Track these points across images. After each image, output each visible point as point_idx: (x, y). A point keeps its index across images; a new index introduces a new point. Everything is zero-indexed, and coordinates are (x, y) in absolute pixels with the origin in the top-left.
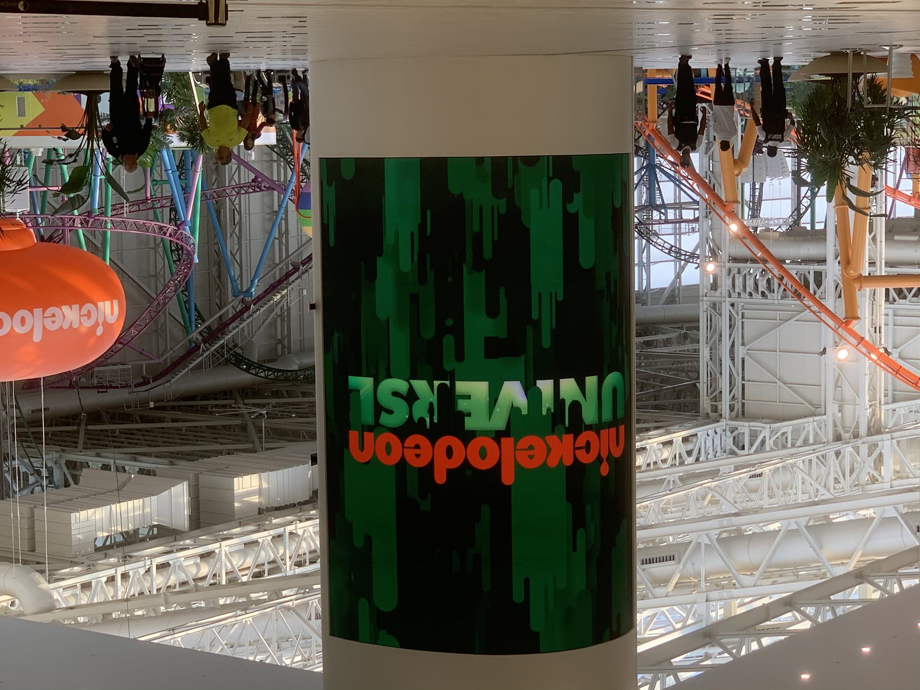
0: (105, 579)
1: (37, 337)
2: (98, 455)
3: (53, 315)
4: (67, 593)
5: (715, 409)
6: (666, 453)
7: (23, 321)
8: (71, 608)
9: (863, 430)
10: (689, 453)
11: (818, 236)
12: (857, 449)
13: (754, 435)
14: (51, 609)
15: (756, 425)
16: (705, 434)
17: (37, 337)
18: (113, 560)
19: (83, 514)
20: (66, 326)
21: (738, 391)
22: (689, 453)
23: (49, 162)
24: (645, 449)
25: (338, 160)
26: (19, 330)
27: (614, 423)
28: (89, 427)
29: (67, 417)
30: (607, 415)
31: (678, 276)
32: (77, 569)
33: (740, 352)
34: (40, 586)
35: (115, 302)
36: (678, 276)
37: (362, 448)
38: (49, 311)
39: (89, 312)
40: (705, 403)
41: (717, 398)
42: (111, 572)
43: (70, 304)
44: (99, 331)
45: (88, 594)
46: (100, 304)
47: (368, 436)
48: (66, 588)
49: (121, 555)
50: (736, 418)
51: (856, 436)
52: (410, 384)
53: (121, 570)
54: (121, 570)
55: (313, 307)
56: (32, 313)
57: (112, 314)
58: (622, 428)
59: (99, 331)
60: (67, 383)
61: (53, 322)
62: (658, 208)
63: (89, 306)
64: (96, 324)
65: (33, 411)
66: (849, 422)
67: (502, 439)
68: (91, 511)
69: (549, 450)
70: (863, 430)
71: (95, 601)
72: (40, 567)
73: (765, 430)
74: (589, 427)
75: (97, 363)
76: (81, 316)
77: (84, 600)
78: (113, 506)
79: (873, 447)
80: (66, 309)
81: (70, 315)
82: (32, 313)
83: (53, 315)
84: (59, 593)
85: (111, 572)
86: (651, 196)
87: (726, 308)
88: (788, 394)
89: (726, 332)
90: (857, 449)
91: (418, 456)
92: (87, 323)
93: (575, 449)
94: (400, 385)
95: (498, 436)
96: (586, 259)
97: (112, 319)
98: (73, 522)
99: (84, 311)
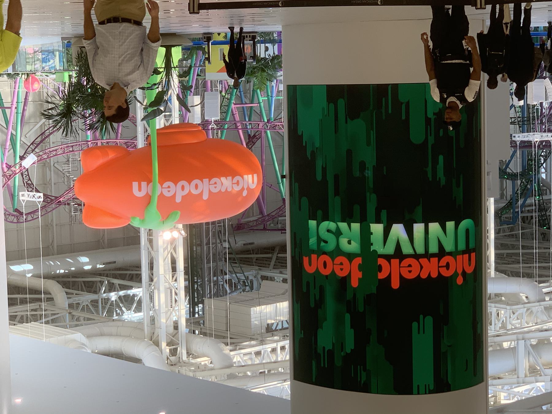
0: (270, 350)
1: (205, 197)
2: (281, 273)
3: (215, 183)
4: (246, 358)
7: (196, 187)
8: (243, 366)
14: (230, 366)
17: (205, 197)
18: (276, 338)
19: (258, 309)
20: (223, 190)
24: (470, 266)
25: (397, 85)
26: (194, 192)
27: (468, 251)
28: (279, 255)
29: (265, 249)
30: (462, 246)
32: (253, 342)
34: (224, 352)
35: (255, 176)
37: (310, 265)
39: (238, 181)
42: (274, 345)
43: (226, 176)
44: (245, 193)
45: (259, 358)
46: (245, 177)
47: (314, 257)
48: (245, 354)
49: (281, 335)
52: (337, 225)
55: (283, 177)
56: (202, 182)
57: (253, 183)
58: (473, 255)
59: (245, 193)
60: (262, 227)
61: (215, 187)
63: (238, 178)
64: (243, 189)
65: (244, 244)
67: (392, 260)
68: (263, 307)
69: (422, 267)
71: (264, 362)
72: (225, 340)
74: (450, 254)
75: (244, 214)
76: (233, 184)
77: (257, 361)
78: (278, 304)
80: (223, 179)
81: (225, 183)
82: (202, 182)
83: (215, 183)
84: (240, 357)
85: (274, 345)
91: (410, 272)
92: (237, 188)
93: (439, 267)
94: (332, 225)
95: (388, 258)
97: (253, 186)
98: (252, 313)
99: (235, 180)
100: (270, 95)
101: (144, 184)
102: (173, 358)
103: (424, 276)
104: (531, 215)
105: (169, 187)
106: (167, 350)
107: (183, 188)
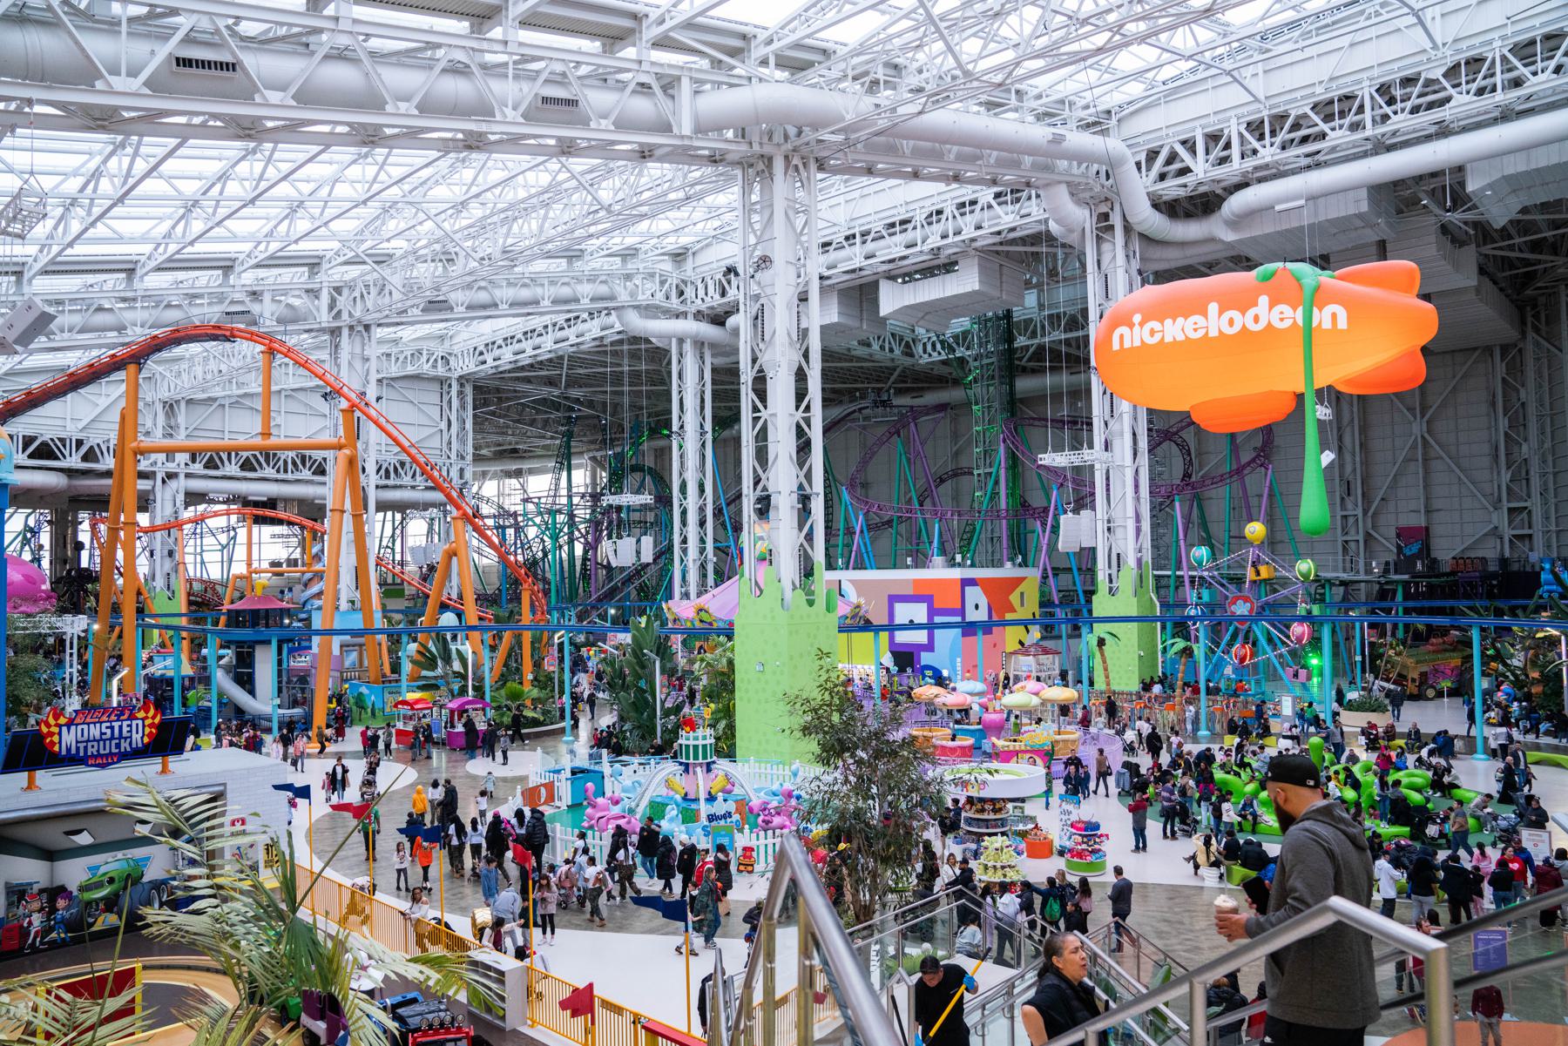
1: (1213, 308)
5: (462, 385)
6: (497, 352)
7: (1231, 322)
9: (345, 332)
10: (481, 353)
11: (382, 507)
12: (350, 315)
13: (434, 366)
15: (432, 373)
16: (468, 366)
17: (1213, 308)
21: (446, 398)
22: (481, 353)
26: (1235, 314)
33: (444, 425)
38: (1200, 333)
40: (469, 390)
41: (460, 393)
44: (1137, 318)
51: (351, 328)
53: (950, 240)
54: (950, 240)
64: (1142, 324)
70: (345, 332)
73: (426, 368)
86: (504, 534)
87: (453, 456)
88: (410, 395)
89: (454, 439)
90: (350, 315)
96: (565, 474)
99: (1158, 337)
102: (1104, 209)
103: (1180, 320)
107: (1256, 319)
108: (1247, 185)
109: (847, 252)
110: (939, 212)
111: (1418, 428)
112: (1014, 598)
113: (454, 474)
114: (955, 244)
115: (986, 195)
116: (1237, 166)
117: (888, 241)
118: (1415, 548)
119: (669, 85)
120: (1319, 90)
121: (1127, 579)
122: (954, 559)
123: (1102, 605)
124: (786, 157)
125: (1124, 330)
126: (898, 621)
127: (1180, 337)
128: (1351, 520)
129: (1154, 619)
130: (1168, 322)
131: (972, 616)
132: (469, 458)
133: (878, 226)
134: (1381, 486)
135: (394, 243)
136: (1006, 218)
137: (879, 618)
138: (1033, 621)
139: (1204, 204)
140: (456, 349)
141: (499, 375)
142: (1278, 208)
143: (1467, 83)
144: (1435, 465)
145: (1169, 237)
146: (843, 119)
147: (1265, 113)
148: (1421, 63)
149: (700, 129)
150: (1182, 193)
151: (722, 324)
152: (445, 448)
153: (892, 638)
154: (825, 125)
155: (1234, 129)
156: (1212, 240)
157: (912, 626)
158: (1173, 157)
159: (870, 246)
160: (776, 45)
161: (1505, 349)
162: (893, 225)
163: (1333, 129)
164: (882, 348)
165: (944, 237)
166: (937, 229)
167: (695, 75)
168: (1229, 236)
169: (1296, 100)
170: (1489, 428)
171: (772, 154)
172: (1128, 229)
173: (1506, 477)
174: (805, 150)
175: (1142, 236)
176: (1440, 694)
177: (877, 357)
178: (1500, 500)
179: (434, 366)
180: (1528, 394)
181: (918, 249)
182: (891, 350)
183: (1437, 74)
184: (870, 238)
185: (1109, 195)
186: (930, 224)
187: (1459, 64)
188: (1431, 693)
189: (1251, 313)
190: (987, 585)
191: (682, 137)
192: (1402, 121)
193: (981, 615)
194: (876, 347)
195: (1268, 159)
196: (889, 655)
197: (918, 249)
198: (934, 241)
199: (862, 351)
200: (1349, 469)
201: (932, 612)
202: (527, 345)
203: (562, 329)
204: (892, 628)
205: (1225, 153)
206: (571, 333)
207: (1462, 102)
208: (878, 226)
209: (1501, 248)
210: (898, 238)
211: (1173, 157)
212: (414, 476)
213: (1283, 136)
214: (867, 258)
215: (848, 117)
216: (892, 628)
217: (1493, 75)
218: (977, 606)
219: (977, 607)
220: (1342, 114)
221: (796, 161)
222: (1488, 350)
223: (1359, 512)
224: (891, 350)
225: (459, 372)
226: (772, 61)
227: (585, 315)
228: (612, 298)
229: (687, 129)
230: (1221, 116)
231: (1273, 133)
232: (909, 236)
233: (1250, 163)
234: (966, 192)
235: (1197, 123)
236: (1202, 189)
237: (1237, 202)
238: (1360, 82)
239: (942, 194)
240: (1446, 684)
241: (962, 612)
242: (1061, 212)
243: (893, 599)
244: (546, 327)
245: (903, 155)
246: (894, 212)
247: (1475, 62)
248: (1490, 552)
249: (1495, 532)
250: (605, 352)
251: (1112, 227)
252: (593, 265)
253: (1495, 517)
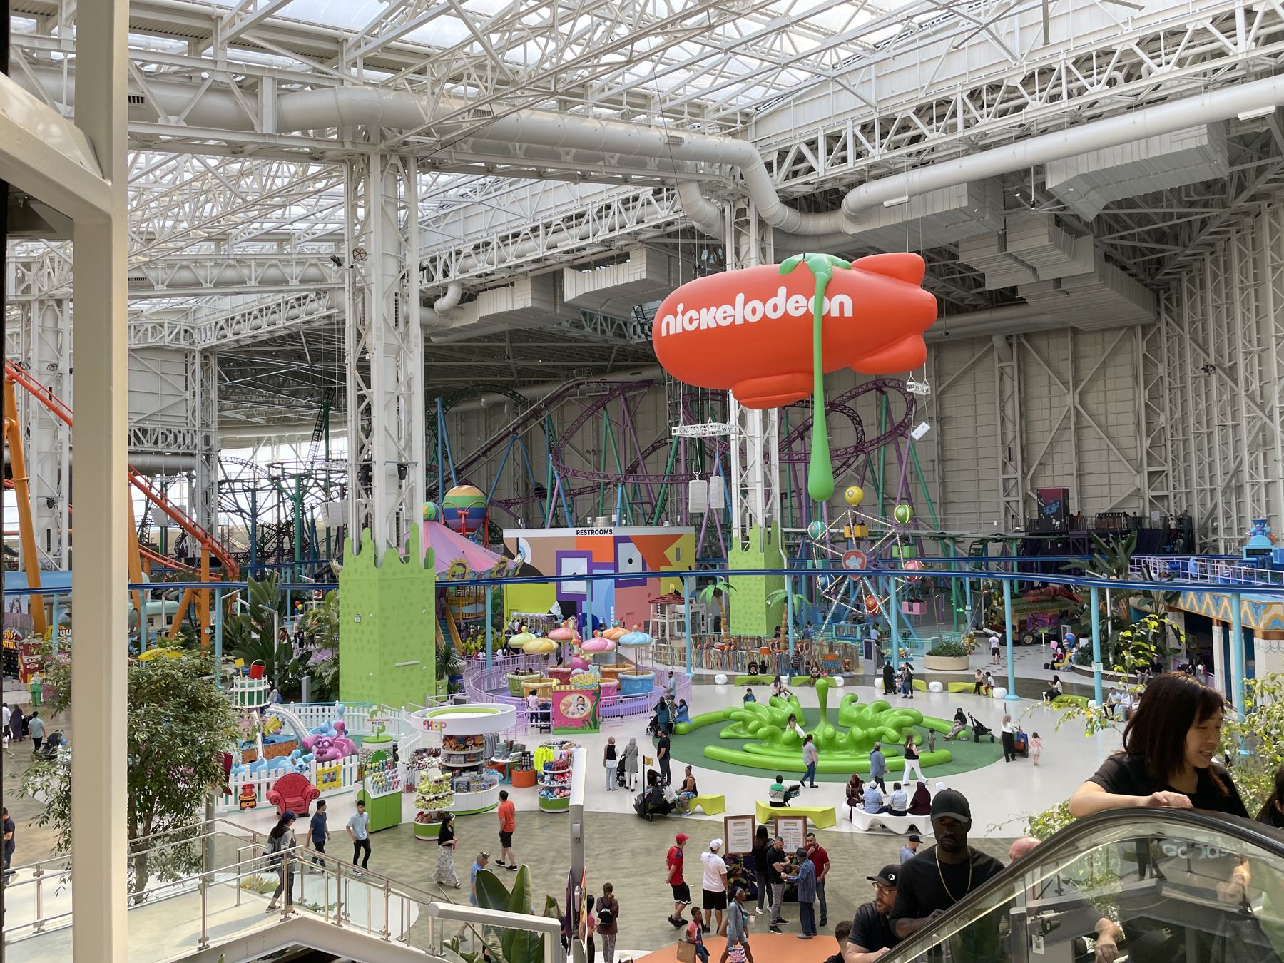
1: (740, 298)
5: (206, 358)
6: (237, 328)
7: (754, 311)
9: (35, 306)
10: (222, 328)
15: (175, 345)
16: (208, 339)
17: (740, 298)
23: (194, 705)
26: (757, 304)
31: (254, 453)
33: (188, 395)
36: (254, 453)
38: (729, 321)
40: (213, 361)
44: (680, 307)
50: (191, 351)
53: (616, 233)
54: (616, 233)
62: (249, 490)
64: (683, 313)
66: (49, 314)
79: (27, 290)
81: (710, 318)
87: (198, 423)
99: (695, 324)
100: (897, 29)
101: (835, 313)
102: (741, 205)
104: (924, 129)
105: (797, 308)
106: (751, 216)
107: (775, 308)
108: (862, 182)
109: (531, 244)
110: (608, 207)
111: (1070, 399)
112: (670, 553)
113: (199, 440)
114: (621, 237)
115: (646, 192)
116: (852, 164)
117: (565, 234)
118: (1054, 509)
119: (250, 87)
120: (921, 95)
121: (755, 535)
122: (610, 519)
123: (736, 559)
124: (383, 157)
125: (670, 318)
126: (563, 574)
127: (713, 325)
128: (1012, 482)
129: (779, 572)
130: (704, 311)
131: (624, 568)
132: (214, 426)
133: (557, 220)
134: (1039, 450)
135: (296, 225)
136: (662, 213)
137: (548, 571)
138: (689, 573)
139: (826, 200)
140: (199, 324)
141: (241, 348)
142: (886, 204)
143: (1041, 91)
144: (1087, 433)
145: (802, 230)
146: (423, 122)
147: (876, 116)
148: (1003, 71)
149: (284, 127)
150: (809, 190)
151: (432, 307)
152: (190, 417)
153: (559, 588)
154: (410, 127)
155: (850, 131)
156: (838, 233)
157: (576, 577)
158: (800, 158)
159: (552, 238)
160: (364, 48)
161: (1146, 328)
162: (570, 218)
163: (931, 131)
164: (595, 329)
165: (612, 230)
166: (606, 222)
167: (278, 76)
168: (852, 229)
169: (901, 104)
170: (1134, 399)
171: (375, 150)
172: (762, 223)
173: (1146, 443)
174: (404, 150)
175: (777, 230)
176: (1038, 641)
177: (592, 338)
178: (1141, 465)
179: (178, 339)
180: (1162, 369)
181: (590, 241)
182: (603, 332)
183: (1016, 82)
184: (551, 230)
185: (745, 193)
186: (600, 218)
187: (1033, 75)
188: (1029, 639)
189: (771, 302)
190: (639, 541)
191: (265, 135)
192: (988, 124)
193: (637, 567)
194: (588, 329)
195: (877, 159)
196: (557, 604)
197: (590, 241)
198: (604, 234)
199: (575, 333)
200: (1010, 436)
201: (591, 566)
202: (262, 322)
203: (293, 307)
204: (559, 579)
205: (843, 153)
206: (301, 312)
207: (1037, 108)
208: (557, 220)
209: (1122, 238)
210: (574, 231)
211: (800, 158)
212: (156, 442)
213: (891, 137)
214: (550, 248)
215: (427, 120)
216: (559, 579)
217: (1060, 85)
218: (631, 560)
219: (630, 561)
220: (941, 117)
221: (395, 160)
222: (1132, 328)
223: (1019, 475)
224: (603, 332)
225: (202, 346)
226: (360, 63)
227: (313, 295)
228: (322, 280)
229: (269, 126)
230: (839, 119)
231: (883, 136)
232: (583, 229)
233: (863, 163)
234: (629, 191)
235: (819, 126)
236: (827, 186)
237: (854, 198)
238: (954, 87)
239: (615, 194)
240: (1043, 632)
241: (616, 565)
242: (696, 207)
243: (561, 554)
244: (279, 305)
245: (516, 157)
246: (571, 206)
247: (1046, 72)
248: (1132, 509)
249: (1138, 493)
250: (333, 330)
251: (748, 222)
252: (238, 250)
253: (1137, 480)
